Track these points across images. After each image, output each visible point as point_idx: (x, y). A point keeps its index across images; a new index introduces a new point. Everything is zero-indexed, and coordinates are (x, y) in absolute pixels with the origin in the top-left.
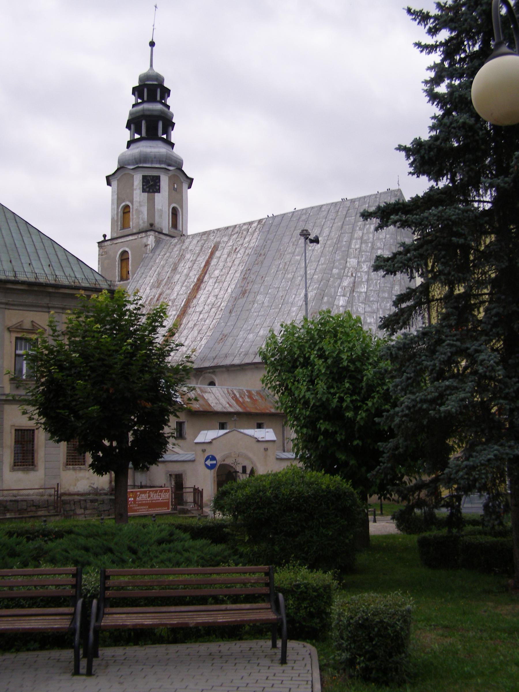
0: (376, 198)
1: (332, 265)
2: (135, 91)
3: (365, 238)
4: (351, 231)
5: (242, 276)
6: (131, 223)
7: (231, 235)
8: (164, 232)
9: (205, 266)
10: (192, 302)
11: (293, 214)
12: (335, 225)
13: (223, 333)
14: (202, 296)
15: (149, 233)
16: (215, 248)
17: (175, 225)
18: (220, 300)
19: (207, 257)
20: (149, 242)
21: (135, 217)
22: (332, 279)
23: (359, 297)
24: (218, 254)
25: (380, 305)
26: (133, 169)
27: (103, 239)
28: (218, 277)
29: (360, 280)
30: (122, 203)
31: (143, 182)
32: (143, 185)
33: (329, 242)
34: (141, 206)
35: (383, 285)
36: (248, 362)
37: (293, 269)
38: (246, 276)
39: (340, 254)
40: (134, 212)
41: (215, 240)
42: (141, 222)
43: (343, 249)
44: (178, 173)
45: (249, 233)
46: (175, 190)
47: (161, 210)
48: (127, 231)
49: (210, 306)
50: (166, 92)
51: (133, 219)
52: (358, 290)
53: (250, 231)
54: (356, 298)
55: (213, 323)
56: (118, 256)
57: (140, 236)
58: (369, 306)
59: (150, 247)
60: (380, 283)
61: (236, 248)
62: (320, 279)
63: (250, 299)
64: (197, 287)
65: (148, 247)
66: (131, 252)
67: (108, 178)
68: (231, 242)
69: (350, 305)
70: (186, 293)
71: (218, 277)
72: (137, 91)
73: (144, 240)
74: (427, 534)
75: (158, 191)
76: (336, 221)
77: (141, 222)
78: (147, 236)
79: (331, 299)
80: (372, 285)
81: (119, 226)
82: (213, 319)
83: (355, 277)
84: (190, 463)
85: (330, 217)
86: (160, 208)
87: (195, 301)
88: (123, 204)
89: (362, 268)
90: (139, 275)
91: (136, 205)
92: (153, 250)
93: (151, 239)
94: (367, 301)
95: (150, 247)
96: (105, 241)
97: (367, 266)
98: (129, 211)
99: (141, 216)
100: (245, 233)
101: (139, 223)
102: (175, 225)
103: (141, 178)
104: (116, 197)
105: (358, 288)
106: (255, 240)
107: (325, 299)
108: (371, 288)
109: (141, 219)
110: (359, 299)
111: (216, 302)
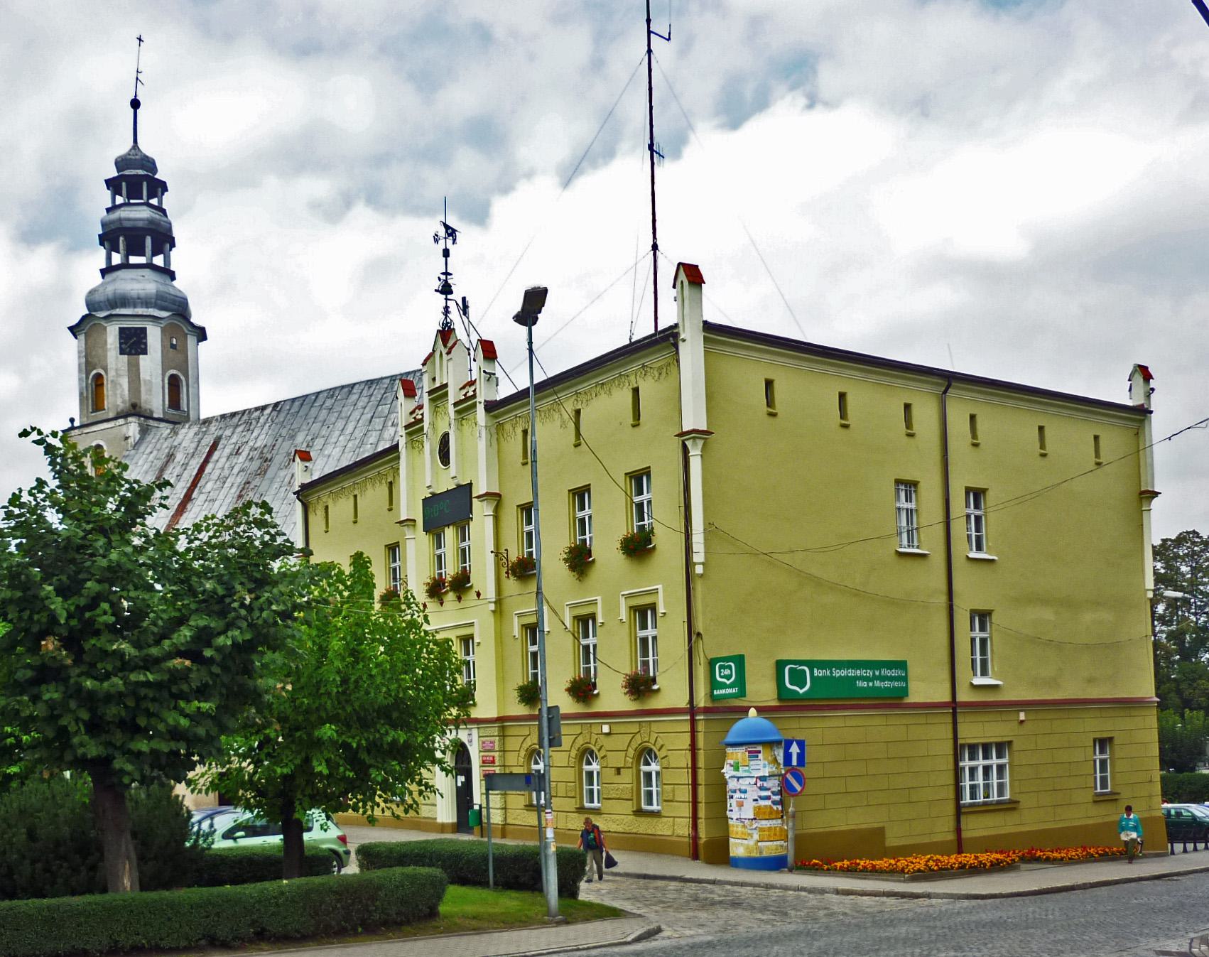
5: (238, 493)
6: (106, 402)
7: (237, 426)
8: (155, 415)
15: (130, 419)
17: (175, 402)
19: (202, 460)
20: (130, 434)
21: (110, 393)
26: (105, 318)
27: (69, 425)
31: (121, 338)
32: (121, 344)
33: (350, 445)
34: (118, 375)
38: (243, 493)
42: (119, 402)
45: (259, 425)
46: (173, 347)
47: (150, 382)
48: (100, 415)
50: (159, 188)
57: (118, 424)
59: (131, 441)
65: (129, 440)
73: (124, 429)
75: (145, 352)
76: (365, 412)
78: (127, 423)
81: (90, 407)
88: (94, 372)
91: (112, 373)
92: (137, 445)
93: (132, 428)
95: (131, 441)
96: (73, 428)
98: (103, 384)
99: (118, 392)
100: (254, 422)
101: (116, 401)
104: (84, 360)
109: (119, 396)
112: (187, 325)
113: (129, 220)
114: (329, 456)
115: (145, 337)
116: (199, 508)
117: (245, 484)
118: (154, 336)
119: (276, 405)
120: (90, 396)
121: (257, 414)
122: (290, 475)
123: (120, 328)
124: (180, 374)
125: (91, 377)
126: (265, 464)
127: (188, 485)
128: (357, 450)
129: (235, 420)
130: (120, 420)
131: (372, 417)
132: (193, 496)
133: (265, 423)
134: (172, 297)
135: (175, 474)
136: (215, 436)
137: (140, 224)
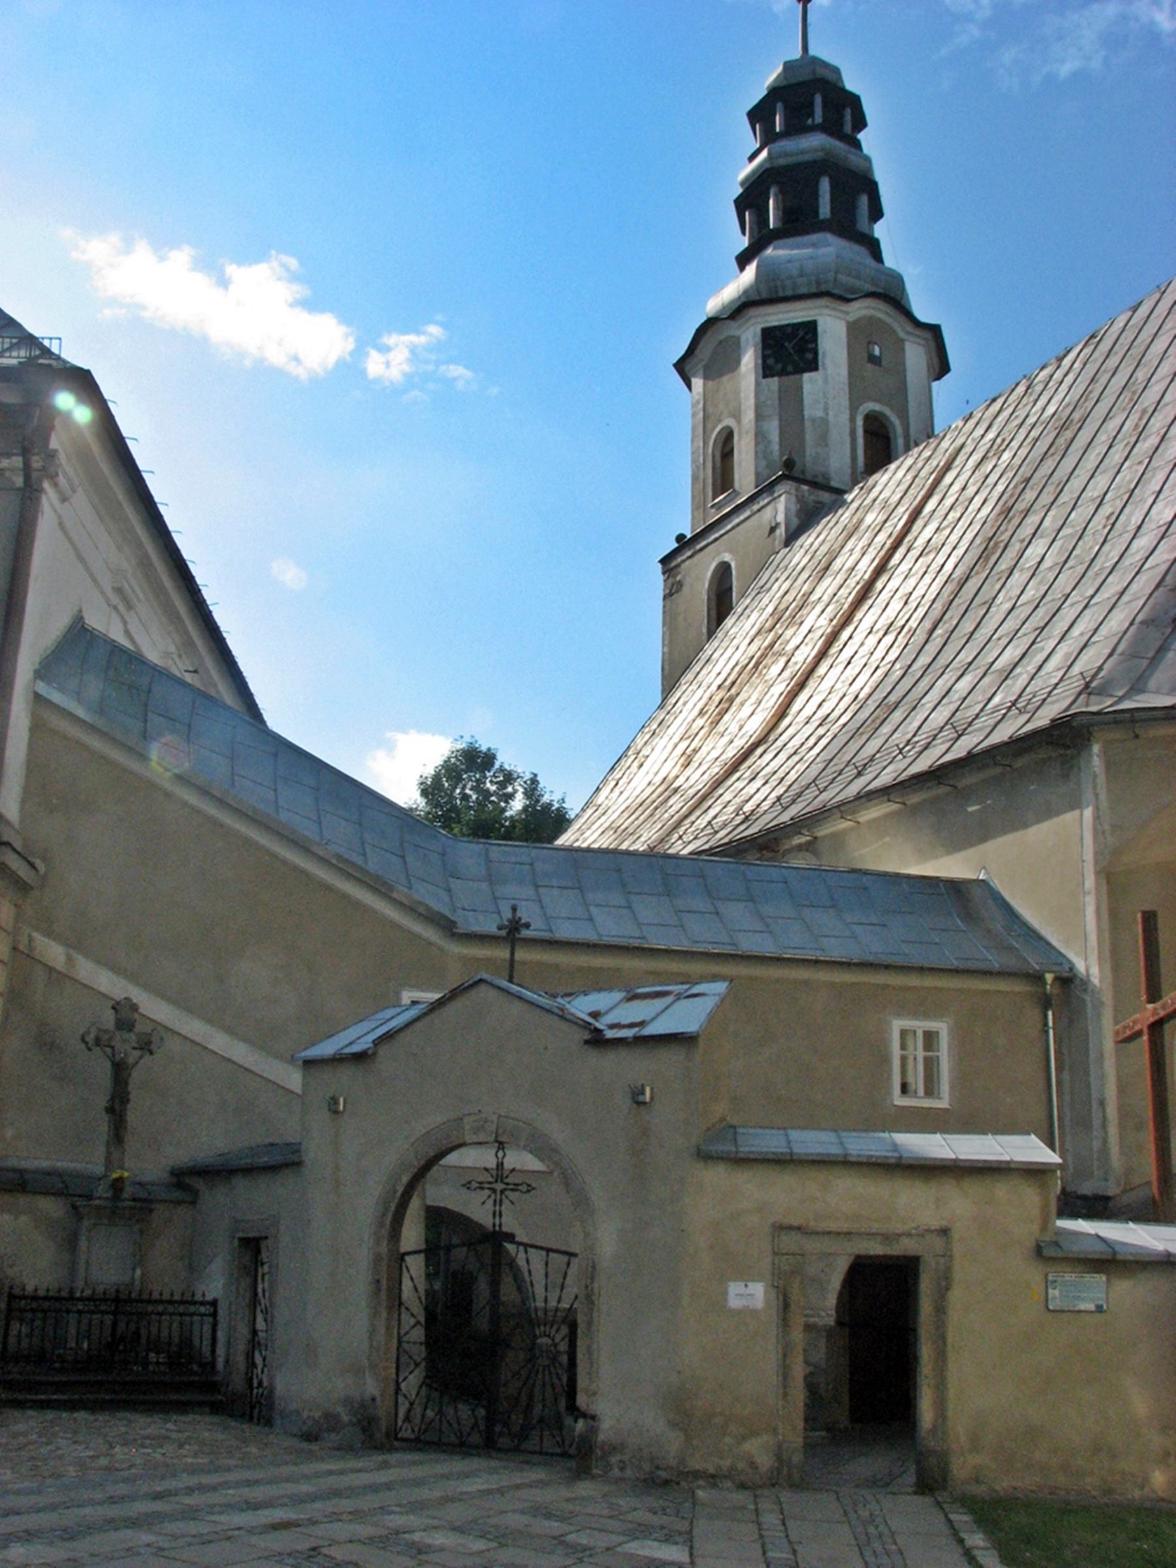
46: (873, 360)
47: (824, 421)
74: (797, 339)
75: (813, 366)
86: (820, 414)
103: (758, 338)
112: (902, 318)
124: (887, 411)
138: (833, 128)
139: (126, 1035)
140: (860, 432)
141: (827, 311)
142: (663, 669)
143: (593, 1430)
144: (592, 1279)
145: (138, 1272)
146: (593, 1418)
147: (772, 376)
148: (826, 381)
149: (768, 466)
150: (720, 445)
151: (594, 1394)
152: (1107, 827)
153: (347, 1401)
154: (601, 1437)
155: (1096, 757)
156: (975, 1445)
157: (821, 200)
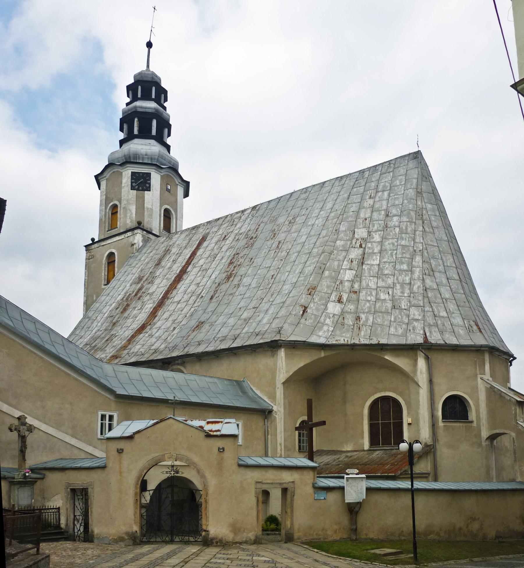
0: (390, 164)
1: (335, 237)
2: (129, 88)
3: (377, 206)
4: (359, 200)
6: (118, 223)
7: (222, 225)
8: (153, 232)
9: (190, 257)
10: (171, 293)
11: (291, 195)
12: (340, 197)
13: (199, 320)
14: (182, 286)
15: (136, 231)
16: (203, 239)
17: (167, 227)
18: (202, 288)
20: (136, 241)
21: (122, 216)
22: (335, 252)
23: (370, 269)
24: (205, 244)
25: (397, 279)
28: (202, 266)
29: (370, 251)
30: (110, 203)
31: (132, 179)
32: (132, 183)
33: (332, 214)
35: (400, 256)
36: (224, 348)
37: (288, 246)
39: (346, 224)
40: (122, 211)
41: (204, 232)
42: (128, 221)
43: (350, 219)
44: (172, 174)
45: (241, 220)
46: (168, 191)
47: (152, 209)
48: (114, 232)
49: (190, 295)
51: (120, 219)
52: (369, 262)
53: (242, 218)
54: (366, 271)
55: (190, 312)
56: (105, 258)
57: (126, 236)
58: (383, 280)
60: (396, 253)
61: (225, 236)
62: (320, 252)
63: (236, 282)
64: (179, 278)
65: (135, 246)
66: (118, 254)
67: (97, 177)
68: (221, 230)
69: (358, 279)
70: (166, 286)
71: (202, 266)
72: (131, 89)
73: (131, 239)
75: (149, 189)
77: (128, 221)
79: (333, 273)
80: (387, 256)
82: (192, 307)
83: (365, 248)
84: (99, 471)
85: (334, 191)
87: (174, 292)
89: (373, 238)
90: (122, 274)
91: (124, 203)
93: (138, 238)
94: (379, 275)
97: (379, 235)
98: (117, 212)
99: (128, 215)
100: (236, 220)
101: (126, 221)
102: (167, 227)
105: (368, 259)
106: (246, 226)
107: (327, 273)
108: (385, 260)
109: (128, 217)
110: (370, 273)
111: (197, 290)
112: (177, 177)
113: (142, 107)
114: (313, 225)
115: (150, 179)
116: (194, 277)
117: (234, 255)
118: (156, 179)
119: (254, 208)
120: (107, 220)
121: (239, 215)
122: (278, 243)
123: (132, 172)
124: (171, 210)
125: (108, 208)
126: (252, 241)
127: (183, 264)
128: (341, 217)
129: (220, 222)
130: (128, 233)
131: (349, 196)
132: (188, 270)
133: (246, 219)
134: (170, 159)
135: (172, 260)
136: (203, 234)
137: (150, 111)
138: (158, 100)
139: (24, 427)
140: (162, 215)
141: (154, 170)
142: (85, 285)
143: (208, 534)
144: (207, 496)
145: (33, 501)
146: (208, 531)
147: (134, 190)
148: (153, 194)
149: (131, 222)
150: (111, 210)
151: (208, 525)
152: (284, 371)
153: (127, 533)
154: (210, 536)
155: (282, 353)
156: (299, 530)
157: (153, 127)
